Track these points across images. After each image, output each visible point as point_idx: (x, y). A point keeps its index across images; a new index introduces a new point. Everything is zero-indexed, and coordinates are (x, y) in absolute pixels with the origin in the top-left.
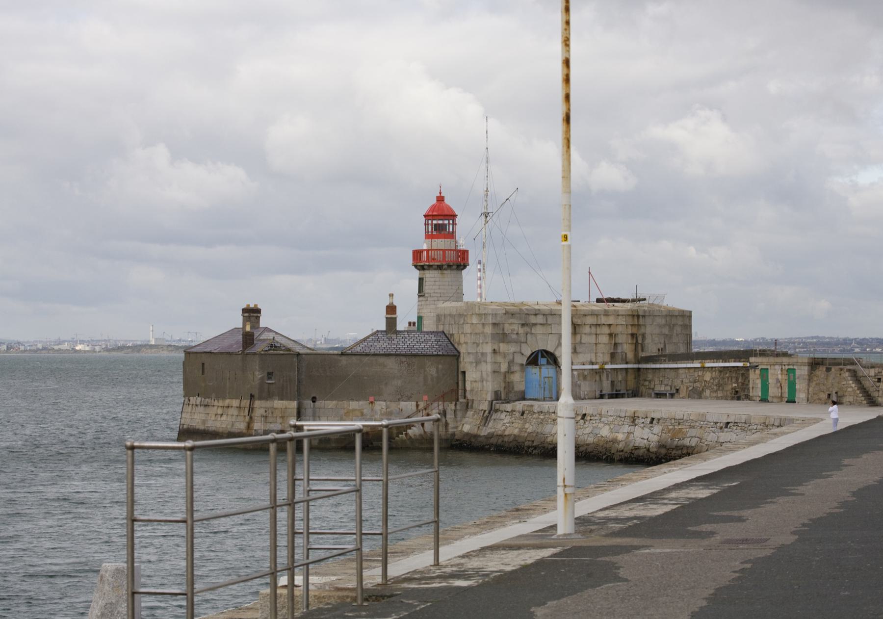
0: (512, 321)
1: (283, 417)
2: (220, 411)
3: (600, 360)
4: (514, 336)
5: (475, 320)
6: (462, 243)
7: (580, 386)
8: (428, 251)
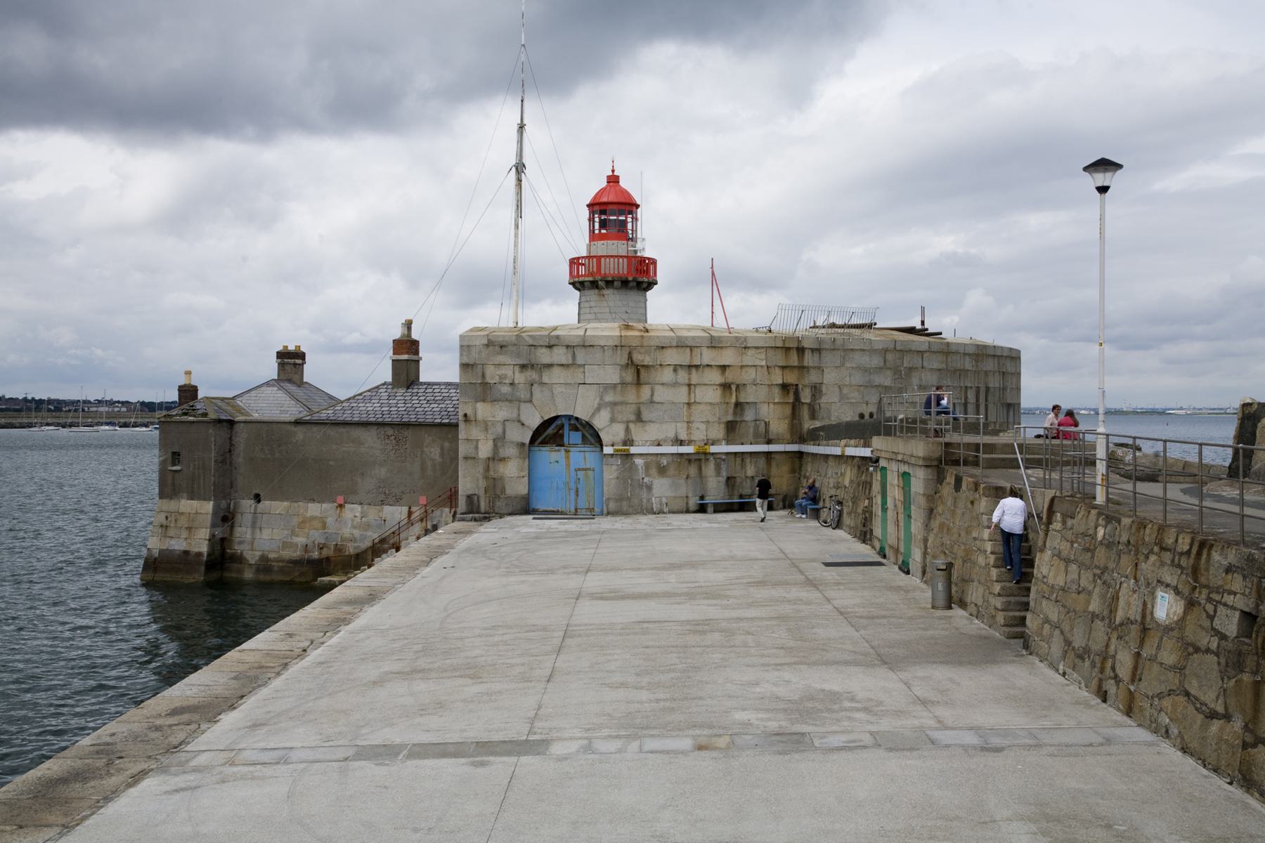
0: (501, 359)
1: (189, 529)
3: (699, 434)
4: (505, 389)
6: (647, 250)
7: (649, 488)
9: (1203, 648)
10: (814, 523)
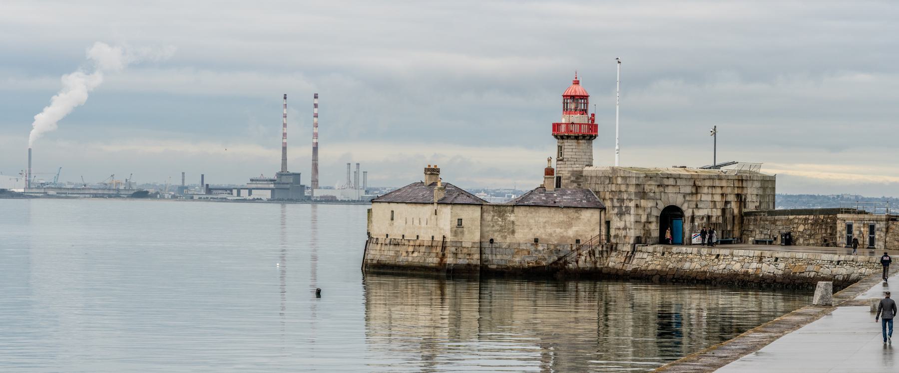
0: (649, 183)
2: (411, 249)
4: (652, 194)
5: (619, 180)
8: (567, 124)
9: (754, 317)
10: (361, 276)
